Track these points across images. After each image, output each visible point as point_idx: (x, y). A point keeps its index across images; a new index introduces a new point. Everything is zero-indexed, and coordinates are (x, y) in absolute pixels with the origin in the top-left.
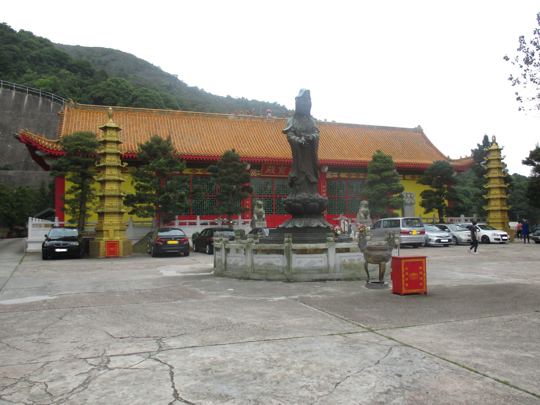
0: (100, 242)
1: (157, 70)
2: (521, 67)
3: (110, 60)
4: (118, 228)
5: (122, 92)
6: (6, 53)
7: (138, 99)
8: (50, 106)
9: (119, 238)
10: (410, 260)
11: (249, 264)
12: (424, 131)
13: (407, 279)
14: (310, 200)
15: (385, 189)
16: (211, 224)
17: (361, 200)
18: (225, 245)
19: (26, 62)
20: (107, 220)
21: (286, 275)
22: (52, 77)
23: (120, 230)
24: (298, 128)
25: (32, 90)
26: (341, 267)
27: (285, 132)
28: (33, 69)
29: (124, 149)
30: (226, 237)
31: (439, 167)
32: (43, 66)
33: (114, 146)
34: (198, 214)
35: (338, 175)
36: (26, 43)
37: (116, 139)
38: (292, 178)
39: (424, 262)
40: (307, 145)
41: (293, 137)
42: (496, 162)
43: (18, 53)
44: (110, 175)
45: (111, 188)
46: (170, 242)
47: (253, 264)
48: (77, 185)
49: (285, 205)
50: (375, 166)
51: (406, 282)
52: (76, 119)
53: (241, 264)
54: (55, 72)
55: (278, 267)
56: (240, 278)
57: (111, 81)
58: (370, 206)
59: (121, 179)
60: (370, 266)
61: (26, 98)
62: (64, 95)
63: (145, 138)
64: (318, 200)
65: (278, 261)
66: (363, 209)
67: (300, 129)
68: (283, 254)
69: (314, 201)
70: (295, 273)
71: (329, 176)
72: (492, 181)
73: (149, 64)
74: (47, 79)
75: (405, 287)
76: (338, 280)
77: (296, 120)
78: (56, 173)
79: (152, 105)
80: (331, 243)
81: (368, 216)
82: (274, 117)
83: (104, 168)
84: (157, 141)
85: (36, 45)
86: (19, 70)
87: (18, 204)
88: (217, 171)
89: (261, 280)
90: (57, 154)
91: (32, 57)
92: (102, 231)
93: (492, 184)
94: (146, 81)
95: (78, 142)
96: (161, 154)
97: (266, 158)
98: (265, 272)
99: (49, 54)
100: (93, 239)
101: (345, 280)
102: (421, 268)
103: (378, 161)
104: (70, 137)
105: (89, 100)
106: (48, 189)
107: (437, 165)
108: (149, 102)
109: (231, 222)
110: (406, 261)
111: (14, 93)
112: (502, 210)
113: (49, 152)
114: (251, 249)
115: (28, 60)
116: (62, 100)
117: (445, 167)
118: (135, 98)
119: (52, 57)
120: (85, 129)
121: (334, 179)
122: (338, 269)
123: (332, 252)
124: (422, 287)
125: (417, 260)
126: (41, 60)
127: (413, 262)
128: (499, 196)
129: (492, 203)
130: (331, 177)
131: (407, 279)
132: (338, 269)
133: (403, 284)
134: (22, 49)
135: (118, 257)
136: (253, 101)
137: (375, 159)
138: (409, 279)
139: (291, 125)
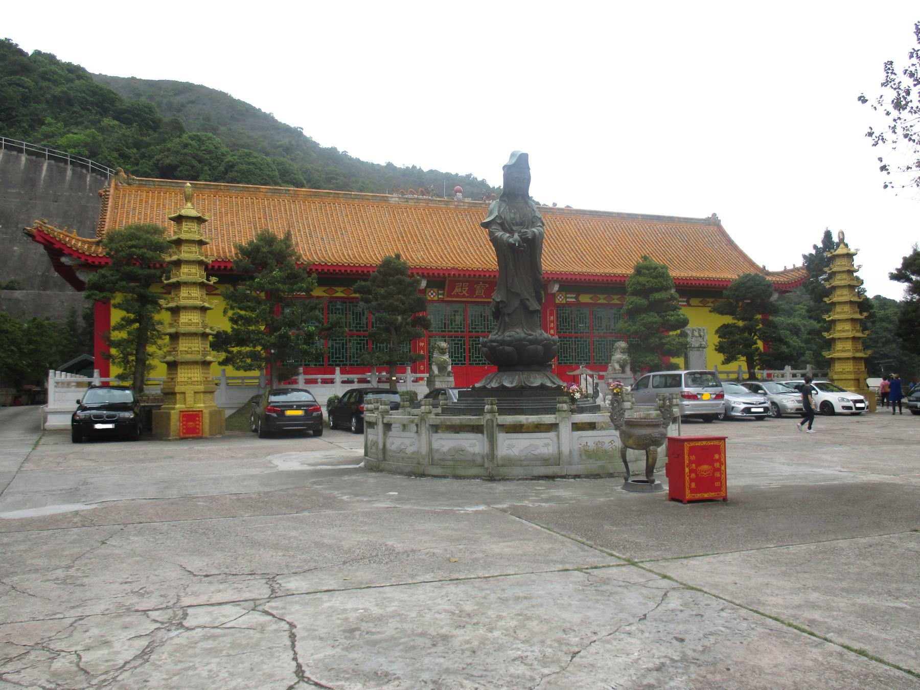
0: (170, 413)
1: (268, 119)
2: (888, 114)
3: (188, 103)
4: (201, 388)
5: (207, 156)
6: (10, 90)
7: (236, 168)
8: (85, 181)
9: (202, 405)
10: (699, 444)
11: (424, 450)
12: (722, 223)
13: (693, 475)
14: (529, 341)
15: (656, 323)
16: (359, 382)
17: (616, 341)
18: (383, 418)
19: (44, 106)
20: (183, 375)
21: (487, 468)
22: (88, 131)
23: (204, 392)
24: (508, 218)
25: (54, 153)
26: (581, 456)
27: (486, 225)
28: (56, 118)
29: (211, 253)
30: (385, 404)
31: (749, 284)
32: (74, 112)
33: (193, 249)
34: (337, 365)
35: (577, 298)
36: (45, 73)
37: (197, 237)
38: (498, 303)
39: (722, 446)
40: (523, 246)
41: (499, 234)
42: (845, 276)
43: (30, 91)
44: (188, 298)
45: (189, 321)
46: (289, 413)
47: (431, 450)
48: (132, 316)
49: (485, 349)
50: (639, 283)
51: (691, 480)
52: (129, 202)
53: (410, 450)
54: (94, 123)
55: (474, 454)
56: (409, 474)
57: (190, 137)
58: (630, 350)
59: (206, 305)
60: (631, 453)
61: (45, 167)
62: (110, 161)
63: (246, 236)
64: (542, 341)
65: (473, 444)
66: (618, 356)
67: (512, 219)
68: (482, 432)
69: (535, 342)
70: (503, 466)
71: (560, 299)
72: (838, 309)
73: (254, 108)
74: (79, 135)
75: (690, 489)
76: (576, 477)
77: (504, 204)
78: (95, 295)
79: (259, 179)
80: (564, 414)
81: (628, 369)
82: (467, 200)
83: (177, 285)
84: (268, 239)
85: (61, 76)
86: (33, 120)
87: (31, 347)
88: (369, 292)
89: (445, 477)
90: (97, 263)
91: (54, 97)
92: (174, 394)
93: (838, 313)
94: (248, 137)
95: (134, 242)
96: (274, 263)
97: (453, 269)
98: (451, 463)
99: (84, 92)
100: (159, 407)
101: (587, 477)
102: (717, 456)
103: (644, 275)
104: (119, 234)
105: (152, 170)
106: (81, 323)
107: (745, 280)
108: (254, 174)
109: (394, 378)
110: (692, 444)
111: (24, 158)
112: (854, 358)
113: (83, 259)
114: (427, 424)
115: (47, 102)
116: (106, 170)
117: (758, 285)
118: (230, 167)
119: (88, 98)
120: (145, 219)
121: (569, 304)
122: (576, 458)
123: (565, 429)
124: (719, 489)
125: (710, 443)
126: (70, 102)
127: (704, 446)
128: (850, 335)
129: (839, 346)
130: (564, 302)
131: (693, 475)
132: (576, 458)
133: (687, 484)
134: (37, 83)
135: (201, 438)
136: (431, 172)
137: (639, 271)
138: (697, 475)
139: (496, 214)
